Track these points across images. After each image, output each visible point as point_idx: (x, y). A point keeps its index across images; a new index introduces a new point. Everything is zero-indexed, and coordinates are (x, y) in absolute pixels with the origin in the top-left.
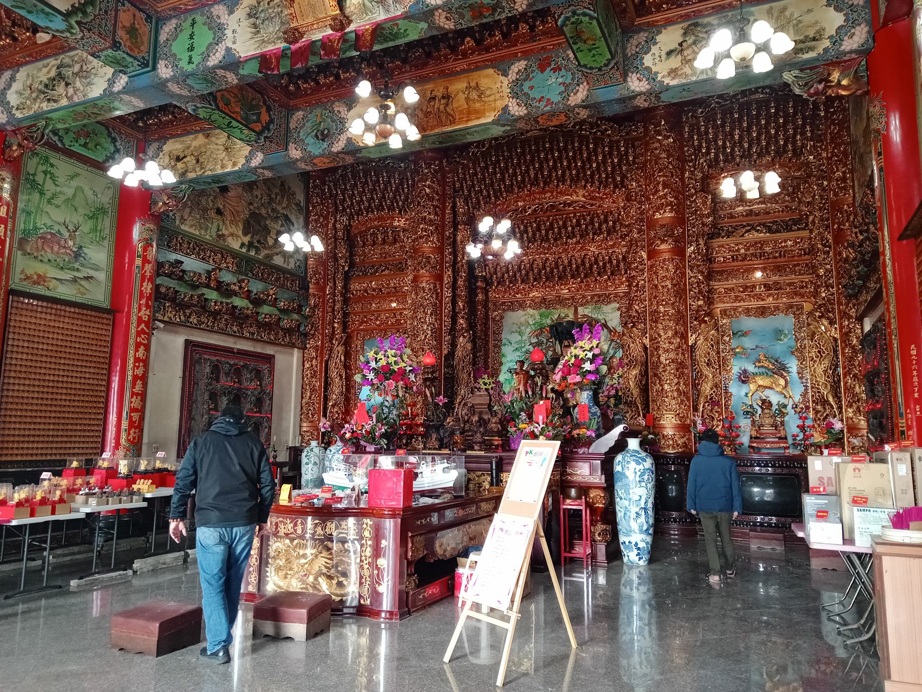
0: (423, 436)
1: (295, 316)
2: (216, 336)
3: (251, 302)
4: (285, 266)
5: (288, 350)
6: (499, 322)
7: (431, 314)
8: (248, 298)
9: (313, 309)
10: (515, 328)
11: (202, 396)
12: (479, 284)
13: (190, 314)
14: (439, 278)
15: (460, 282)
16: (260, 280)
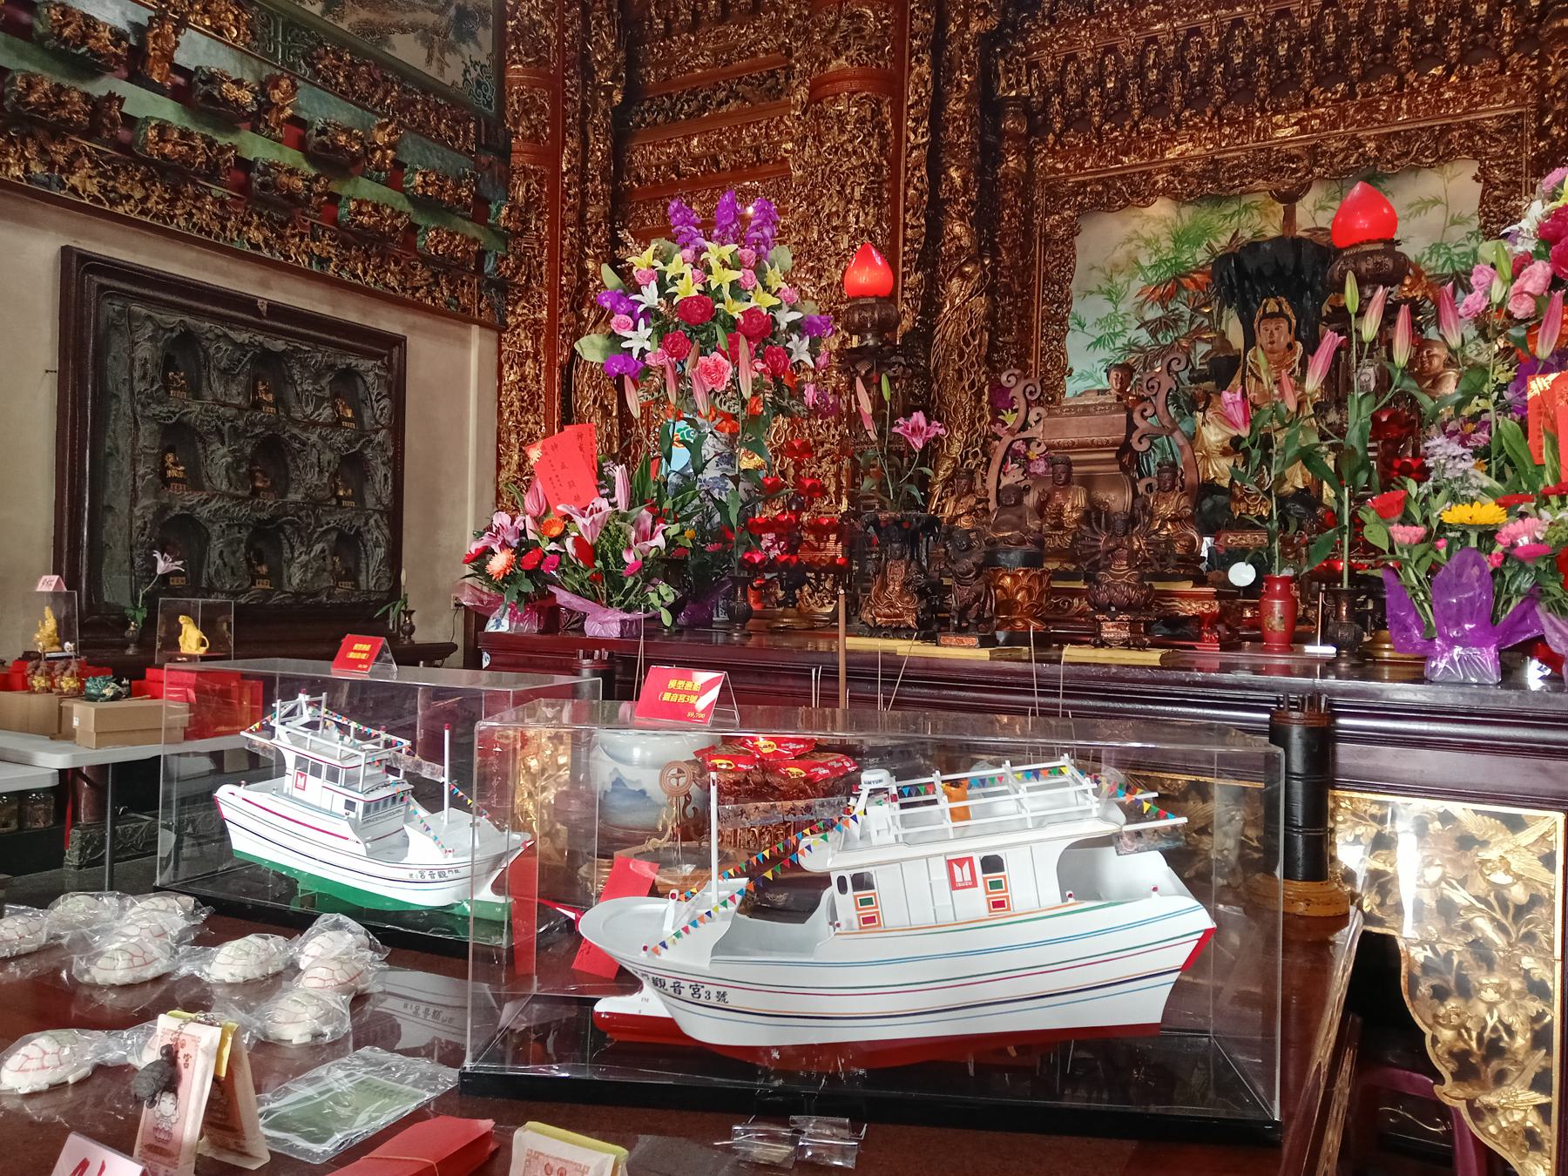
0: (839, 572)
1: (472, 230)
2: (191, 254)
3: (312, 159)
4: (432, 71)
5: (454, 328)
6: (1063, 251)
7: (864, 202)
8: (301, 145)
9: (522, 212)
10: (1097, 279)
11: (132, 441)
12: (1009, 124)
13: (70, 163)
14: (891, 85)
15: (955, 106)
16: (343, 95)
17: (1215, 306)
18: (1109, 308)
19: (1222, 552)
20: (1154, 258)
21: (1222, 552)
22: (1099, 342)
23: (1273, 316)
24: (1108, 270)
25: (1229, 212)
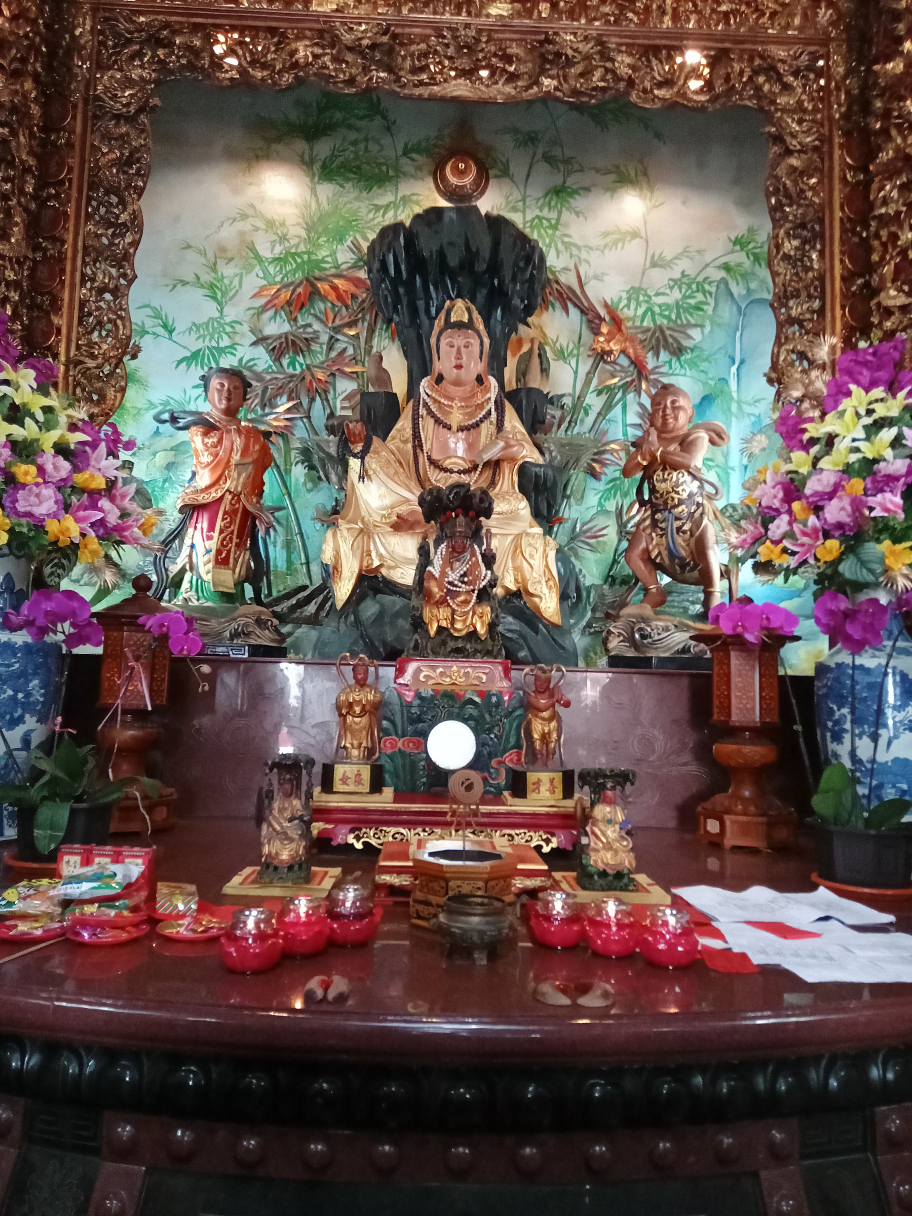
10: (192, 265)
17: (362, 329)
18: (211, 309)
19: (409, 696)
20: (278, 249)
21: (409, 696)
22: (195, 357)
23: (460, 325)
24: (210, 255)
25: (382, 201)
